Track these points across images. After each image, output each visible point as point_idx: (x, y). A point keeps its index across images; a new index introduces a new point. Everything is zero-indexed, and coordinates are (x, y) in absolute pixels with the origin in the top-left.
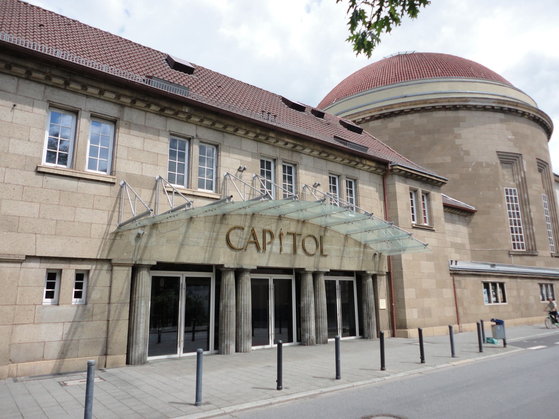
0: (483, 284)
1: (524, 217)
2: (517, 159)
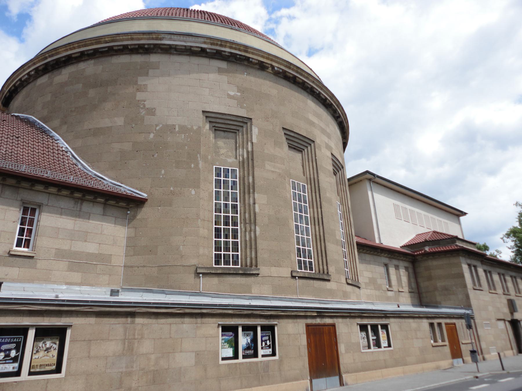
0: (359, 326)
1: (245, 213)
2: (245, 126)
